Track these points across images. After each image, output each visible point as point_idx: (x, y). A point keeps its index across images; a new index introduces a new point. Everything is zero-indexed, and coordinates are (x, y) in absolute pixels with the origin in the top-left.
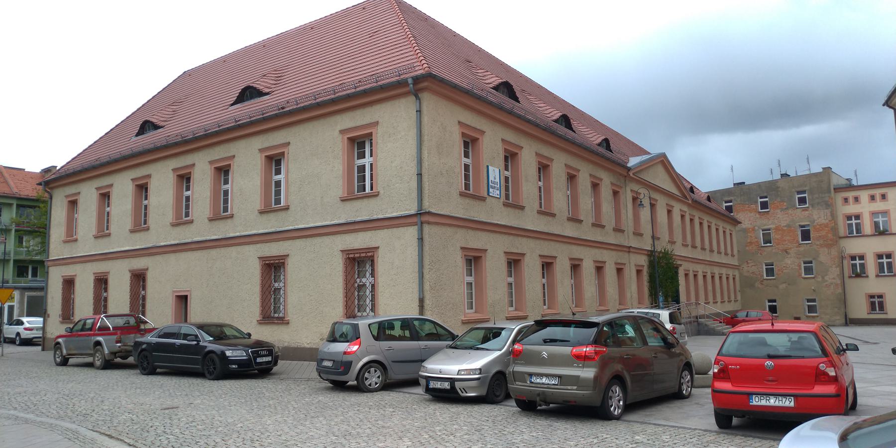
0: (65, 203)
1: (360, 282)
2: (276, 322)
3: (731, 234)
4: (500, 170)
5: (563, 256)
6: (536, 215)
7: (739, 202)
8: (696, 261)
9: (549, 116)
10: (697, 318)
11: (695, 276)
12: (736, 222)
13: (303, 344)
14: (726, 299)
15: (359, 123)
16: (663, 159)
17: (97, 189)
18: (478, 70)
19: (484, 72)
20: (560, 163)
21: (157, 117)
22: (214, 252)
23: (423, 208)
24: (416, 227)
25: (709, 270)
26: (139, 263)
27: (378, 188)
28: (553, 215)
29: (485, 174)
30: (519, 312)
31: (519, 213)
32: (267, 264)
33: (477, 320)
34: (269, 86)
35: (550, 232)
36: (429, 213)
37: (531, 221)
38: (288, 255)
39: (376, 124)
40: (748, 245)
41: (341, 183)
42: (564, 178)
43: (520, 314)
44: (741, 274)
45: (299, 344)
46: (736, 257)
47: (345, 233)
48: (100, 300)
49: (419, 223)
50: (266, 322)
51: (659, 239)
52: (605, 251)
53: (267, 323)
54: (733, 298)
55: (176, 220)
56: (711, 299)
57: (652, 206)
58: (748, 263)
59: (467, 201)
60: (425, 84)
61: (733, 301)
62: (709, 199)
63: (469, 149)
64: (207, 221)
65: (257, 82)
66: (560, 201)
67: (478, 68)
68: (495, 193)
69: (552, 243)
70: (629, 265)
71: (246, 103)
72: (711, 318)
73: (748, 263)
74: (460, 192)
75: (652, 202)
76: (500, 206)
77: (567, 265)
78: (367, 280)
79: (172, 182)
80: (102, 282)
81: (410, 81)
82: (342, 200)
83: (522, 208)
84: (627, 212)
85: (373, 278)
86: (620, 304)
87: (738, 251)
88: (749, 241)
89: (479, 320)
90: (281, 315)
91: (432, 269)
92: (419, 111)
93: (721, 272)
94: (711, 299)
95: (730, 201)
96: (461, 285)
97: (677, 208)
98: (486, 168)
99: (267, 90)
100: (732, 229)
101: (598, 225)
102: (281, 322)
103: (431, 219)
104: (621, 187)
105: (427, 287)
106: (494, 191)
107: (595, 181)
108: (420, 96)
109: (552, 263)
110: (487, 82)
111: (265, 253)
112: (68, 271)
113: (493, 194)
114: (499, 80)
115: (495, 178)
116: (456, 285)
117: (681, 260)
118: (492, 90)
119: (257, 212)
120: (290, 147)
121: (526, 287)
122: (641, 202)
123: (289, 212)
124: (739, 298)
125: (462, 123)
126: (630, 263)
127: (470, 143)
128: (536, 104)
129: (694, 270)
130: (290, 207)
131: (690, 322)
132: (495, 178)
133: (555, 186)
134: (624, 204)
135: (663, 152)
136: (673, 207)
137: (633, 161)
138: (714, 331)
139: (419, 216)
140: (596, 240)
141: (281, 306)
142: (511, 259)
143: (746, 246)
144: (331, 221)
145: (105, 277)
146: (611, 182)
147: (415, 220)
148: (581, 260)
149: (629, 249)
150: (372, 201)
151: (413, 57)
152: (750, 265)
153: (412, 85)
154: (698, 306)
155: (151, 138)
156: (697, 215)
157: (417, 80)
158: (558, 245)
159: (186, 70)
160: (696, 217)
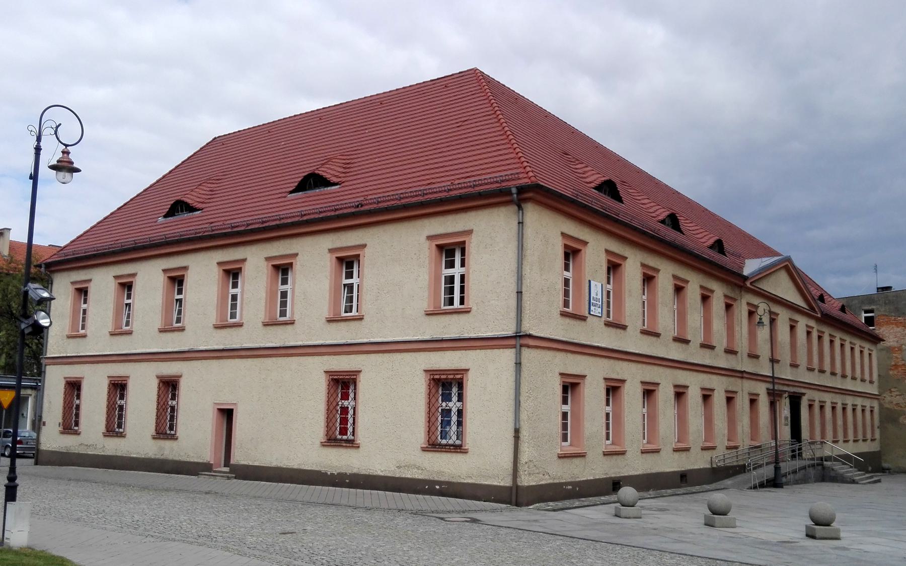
0: (71, 289)
1: (446, 407)
2: (344, 445)
3: (870, 354)
4: (602, 285)
5: (666, 380)
6: (639, 335)
7: (883, 313)
8: (823, 389)
9: (655, 216)
10: (822, 460)
11: (822, 407)
12: (876, 339)
13: (376, 471)
14: (860, 437)
15: (450, 230)
16: (787, 263)
17: (116, 277)
18: (577, 164)
19: (584, 167)
20: (667, 273)
21: (192, 197)
22: (269, 361)
23: (523, 329)
24: (513, 350)
25: (839, 400)
26: (169, 369)
27: (470, 302)
28: (657, 335)
29: (587, 290)
30: (617, 447)
31: (621, 333)
32: (335, 379)
33: (573, 455)
34: (337, 174)
35: (653, 355)
36: (530, 336)
37: (633, 342)
38: (360, 371)
39: (470, 232)
40: (893, 368)
41: (426, 294)
42: (670, 289)
43: (617, 448)
44: (881, 405)
45: (372, 471)
46: (876, 384)
47: (430, 351)
48: (72, 408)
49: (518, 346)
50: (332, 444)
51: (778, 361)
52: (714, 377)
53: (333, 445)
54: (869, 436)
55: (221, 321)
56: (841, 437)
57: (772, 321)
58: (891, 392)
59: (568, 321)
60: (530, 195)
61: (869, 440)
62: (843, 309)
63: (569, 261)
64: (260, 325)
66: (666, 322)
67: (577, 162)
68: (596, 311)
69: (656, 368)
70: (741, 393)
71: (310, 193)
72: (838, 461)
73: (891, 392)
74: (560, 311)
75: (772, 316)
76: (601, 326)
77: (671, 392)
78: (454, 405)
79: (217, 277)
80: (118, 387)
81: (514, 190)
82: (427, 314)
83: (624, 327)
84: (741, 330)
85: (462, 403)
86: (728, 440)
87: (879, 376)
88: (893, 363)
89: (576, 455)
91: (530, 397)
92: (521, 223)
93: (855, 403)
94: (841, 437)
95: (871, 311)
96: (558, 415)
97: (803, 323)
98: (588, 282)
99: (335, 180)
100: (872, 348)
101: (707, 346)
102: (351, 445)
103: (531, 342)
104: (735, 300)
105: (524, 416)
106: (595, 309)
107: (705, 293)
108: (522, 206)
109: (653, 391)
110: (588, 180)
111: (333, 367)
112: (74, 372)
114: (601, 177)
115: (597, 295)
116: (553, 415)
117: (805, 388)
118: (594, 190)
119: (324, 320)
120: (366, 249)
121: (625, 418)
122: (760, 319)
123: (363, 322)
124: (877, 435)
125: (566, 234)
126: (742, 390)
127: (571, 253)
128: (639, 200)
129: (821, 400)
130: (365, 317)
131: (813, 466)
132: (597, 295)
133: (660, 300)
134: (738, 319)
135: (788, 255)
136: (797, 322)
137: (750, 267)
138: (843, 478)
139: (518, 339)
140: (704, 363)
142: (609, 386)
143: (891, 369)
144: (414, 336)
145: (123, 382)
146: (724, 293)
147: (512, 342)
148: (686, 387)
149: (742, 375)
150: (463, 318)
151: (512, 161)
152: (893, 394)
153: (515, 195)
154: (824, 445)
155: (183, 224)
156: (827, 331)
157: (521, 190)
158: (661, 370)
159: (217, 136)
160: (825, 334)
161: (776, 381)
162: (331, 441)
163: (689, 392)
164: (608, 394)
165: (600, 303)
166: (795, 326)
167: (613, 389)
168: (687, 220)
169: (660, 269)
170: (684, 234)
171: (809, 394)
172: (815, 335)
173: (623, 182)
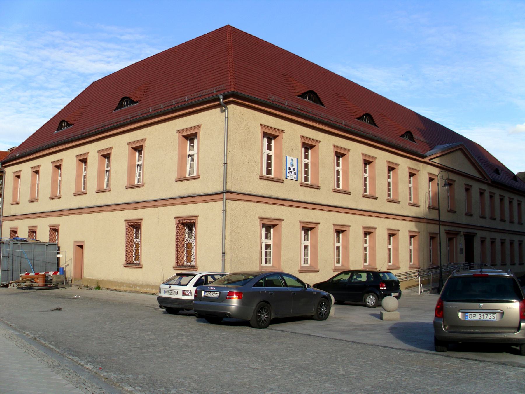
27: (112, 186)
64: (95, 192)
65: (131, 94)
90: (193, 264)
97: (476, 187)
106: (291, 175)
113: (291, 178)
132: (293, 166)
141: (192, 256)
156: (498, 193)
161: (441, 223)
162: (129, 264)
163: (377, 232)
164: (430, 239)
165: (296, 171)
166: (483, 193)
167: (368, 233)
168: (392, 120)
169: (350, 149)
170: (377, 126)
171: (480, 234)
172: (487, 195)
173: (337, 94)
